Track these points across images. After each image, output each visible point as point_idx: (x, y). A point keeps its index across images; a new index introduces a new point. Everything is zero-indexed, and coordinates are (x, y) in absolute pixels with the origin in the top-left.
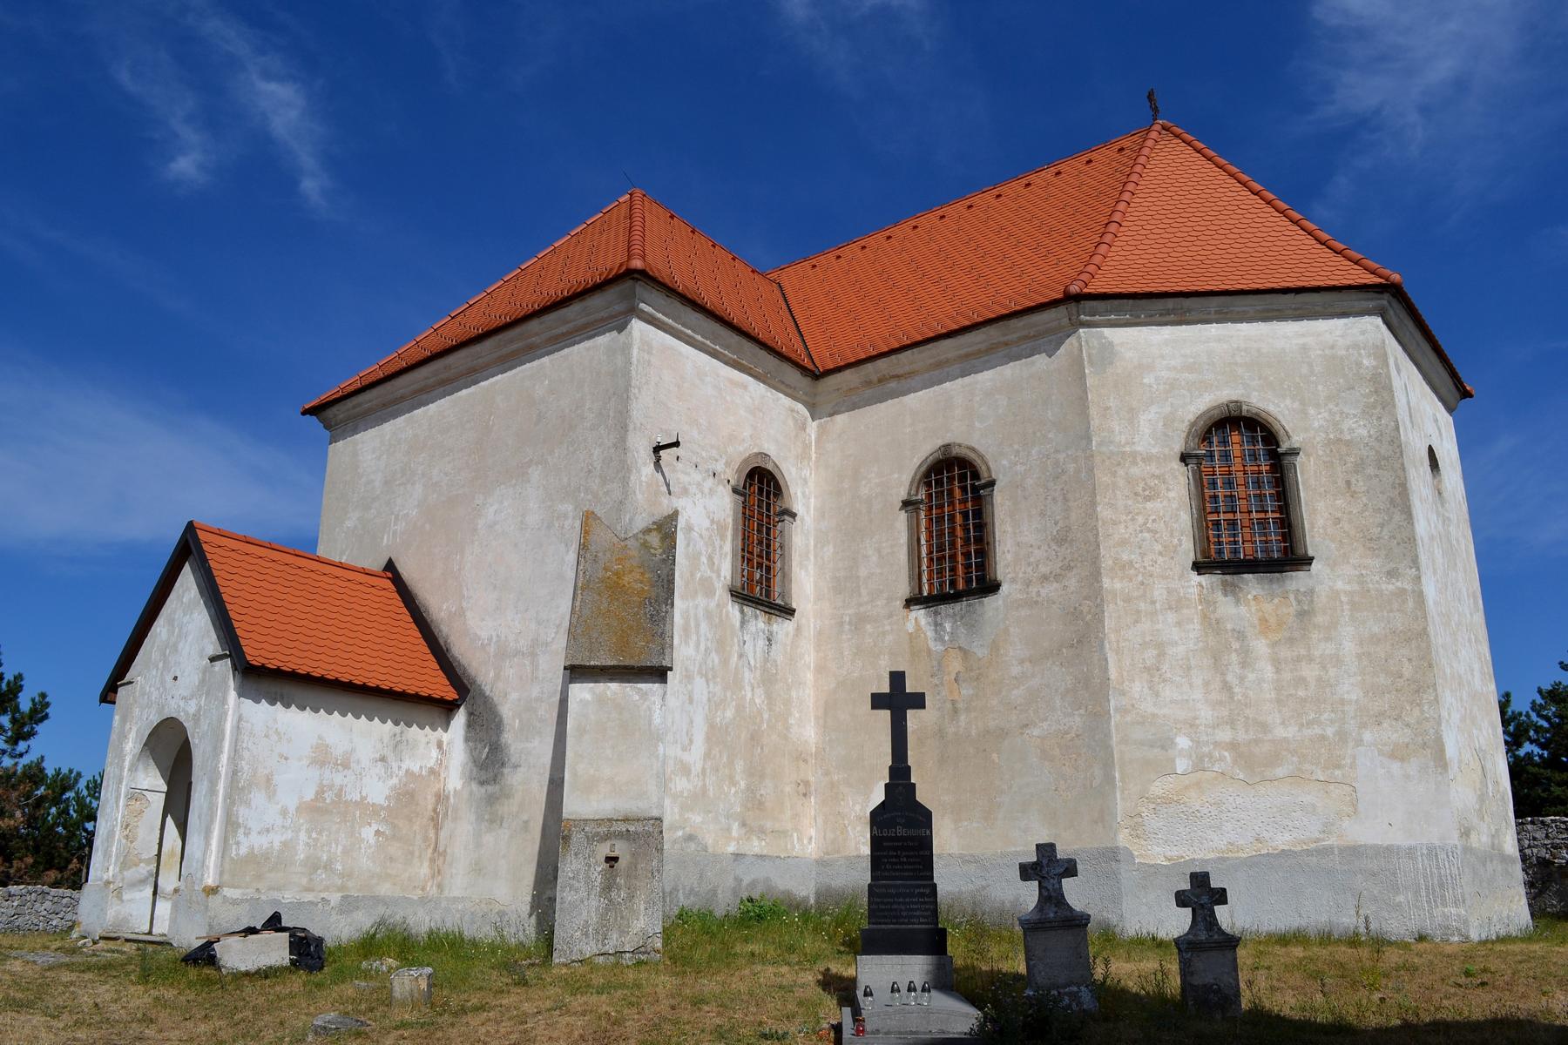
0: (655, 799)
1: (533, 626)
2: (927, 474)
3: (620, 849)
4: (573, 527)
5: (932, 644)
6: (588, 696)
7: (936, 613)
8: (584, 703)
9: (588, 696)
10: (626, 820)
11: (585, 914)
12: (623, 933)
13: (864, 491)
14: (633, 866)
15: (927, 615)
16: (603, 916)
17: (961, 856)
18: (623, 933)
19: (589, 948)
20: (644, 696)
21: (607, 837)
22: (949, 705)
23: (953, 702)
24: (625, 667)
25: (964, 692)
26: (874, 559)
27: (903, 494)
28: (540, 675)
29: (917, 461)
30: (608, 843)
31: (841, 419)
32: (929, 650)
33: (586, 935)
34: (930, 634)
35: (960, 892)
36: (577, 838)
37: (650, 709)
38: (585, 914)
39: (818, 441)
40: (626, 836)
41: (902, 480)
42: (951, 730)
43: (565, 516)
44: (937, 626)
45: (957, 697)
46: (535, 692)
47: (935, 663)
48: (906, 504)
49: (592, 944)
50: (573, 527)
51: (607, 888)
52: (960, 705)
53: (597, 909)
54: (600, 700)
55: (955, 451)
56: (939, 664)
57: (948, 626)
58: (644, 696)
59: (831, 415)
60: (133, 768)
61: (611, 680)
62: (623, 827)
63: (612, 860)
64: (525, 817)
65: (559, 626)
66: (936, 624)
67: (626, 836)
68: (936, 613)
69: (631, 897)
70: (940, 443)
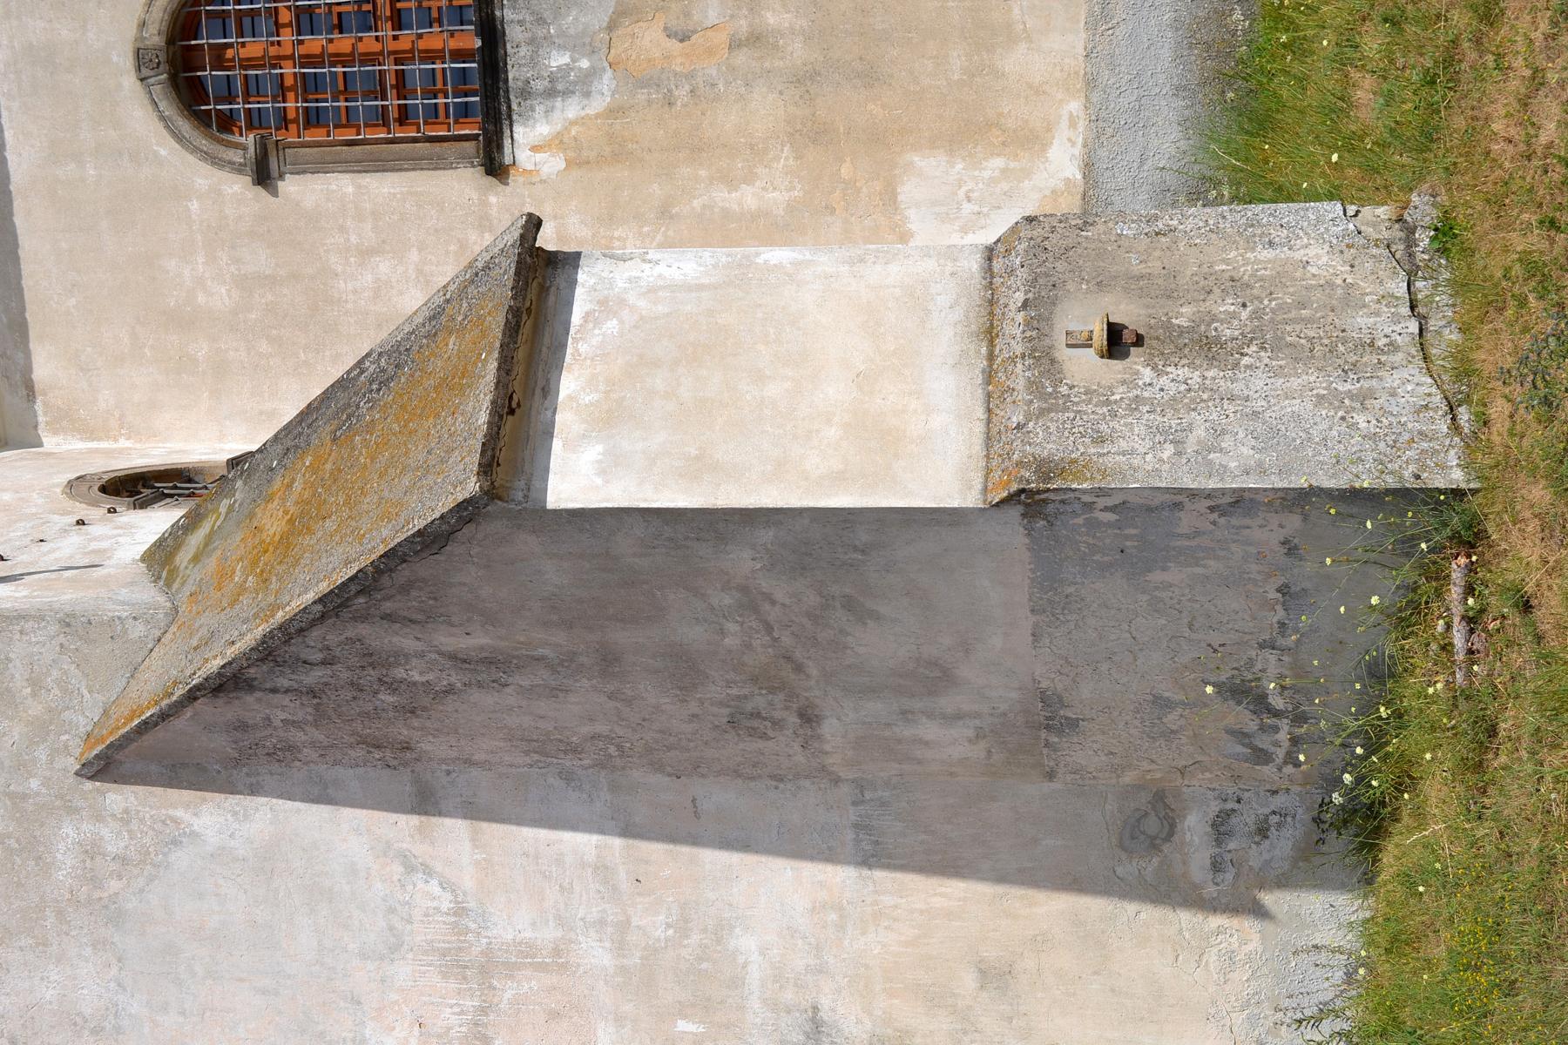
0: (930, 264)
1: (402, 971)
2: (202, 120)
3: (1084, 316)
4: (125, 818)
5: (597, 105)
6: (592, 453)
7: (526, 93)
8: (610, 466)
9: (592, 453)
10: (990, 334)
11: (1295, 406)
12: (1350, 299)
13: (220, 297)
14: (1137, 284)
15: (527, 118)
16: (1302, 356)
17: (1091, 26)
18: (1350, 299)
19: (1409, 387)
20: (607, 306)
21: (1043, 359)
22: (741, 58)
23: (735, 44)
24: (512, 329)
25: (713, 16)
26: (384, 266)
27: (238, 186)
28: (549, 934)
29: (165, 148)
30: (1063, 354)
31: (45, 366)
32: (613, 112)
33: (1363, 398)
34: (571, 109)
35: (1176, 24)
36: (1047, 441)
37: (652, 290)
38: (1295, 406)
39: (89, 433)
40: (1039, 309)
41: (212, 187)
42: (798, 52)
43: (91, 850)
44: (555, 90)
45: (721, 38)
46: (596, 954)
47: (642, 96)
48: (263, 176)
49: (1392, 380)
50: (125, 818)
51: (1207, 346)
52: (743, 26)
53: (1276, 373)
54: (607, 419)
55: (155, 37)
56: (643, 83)
57: (558, 60)
58: (607, 306)
59: (30, 390)
60: (289, 8)
61: (548, 391)
62: (1014, 326)
63: (1117, 342)
64: (969, 980)
65: (410, 866)
66: (551, 93)
67: (1039, 309)
68: (526, 93)
69: (1234, 285)
70: (129, 81)
